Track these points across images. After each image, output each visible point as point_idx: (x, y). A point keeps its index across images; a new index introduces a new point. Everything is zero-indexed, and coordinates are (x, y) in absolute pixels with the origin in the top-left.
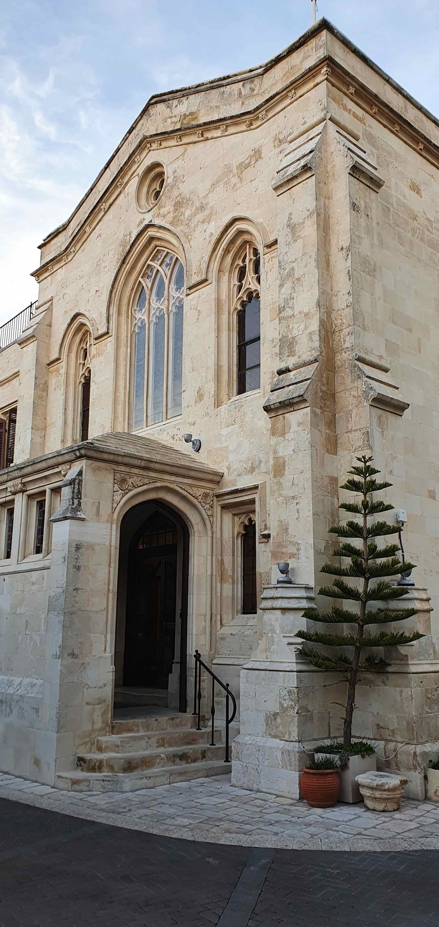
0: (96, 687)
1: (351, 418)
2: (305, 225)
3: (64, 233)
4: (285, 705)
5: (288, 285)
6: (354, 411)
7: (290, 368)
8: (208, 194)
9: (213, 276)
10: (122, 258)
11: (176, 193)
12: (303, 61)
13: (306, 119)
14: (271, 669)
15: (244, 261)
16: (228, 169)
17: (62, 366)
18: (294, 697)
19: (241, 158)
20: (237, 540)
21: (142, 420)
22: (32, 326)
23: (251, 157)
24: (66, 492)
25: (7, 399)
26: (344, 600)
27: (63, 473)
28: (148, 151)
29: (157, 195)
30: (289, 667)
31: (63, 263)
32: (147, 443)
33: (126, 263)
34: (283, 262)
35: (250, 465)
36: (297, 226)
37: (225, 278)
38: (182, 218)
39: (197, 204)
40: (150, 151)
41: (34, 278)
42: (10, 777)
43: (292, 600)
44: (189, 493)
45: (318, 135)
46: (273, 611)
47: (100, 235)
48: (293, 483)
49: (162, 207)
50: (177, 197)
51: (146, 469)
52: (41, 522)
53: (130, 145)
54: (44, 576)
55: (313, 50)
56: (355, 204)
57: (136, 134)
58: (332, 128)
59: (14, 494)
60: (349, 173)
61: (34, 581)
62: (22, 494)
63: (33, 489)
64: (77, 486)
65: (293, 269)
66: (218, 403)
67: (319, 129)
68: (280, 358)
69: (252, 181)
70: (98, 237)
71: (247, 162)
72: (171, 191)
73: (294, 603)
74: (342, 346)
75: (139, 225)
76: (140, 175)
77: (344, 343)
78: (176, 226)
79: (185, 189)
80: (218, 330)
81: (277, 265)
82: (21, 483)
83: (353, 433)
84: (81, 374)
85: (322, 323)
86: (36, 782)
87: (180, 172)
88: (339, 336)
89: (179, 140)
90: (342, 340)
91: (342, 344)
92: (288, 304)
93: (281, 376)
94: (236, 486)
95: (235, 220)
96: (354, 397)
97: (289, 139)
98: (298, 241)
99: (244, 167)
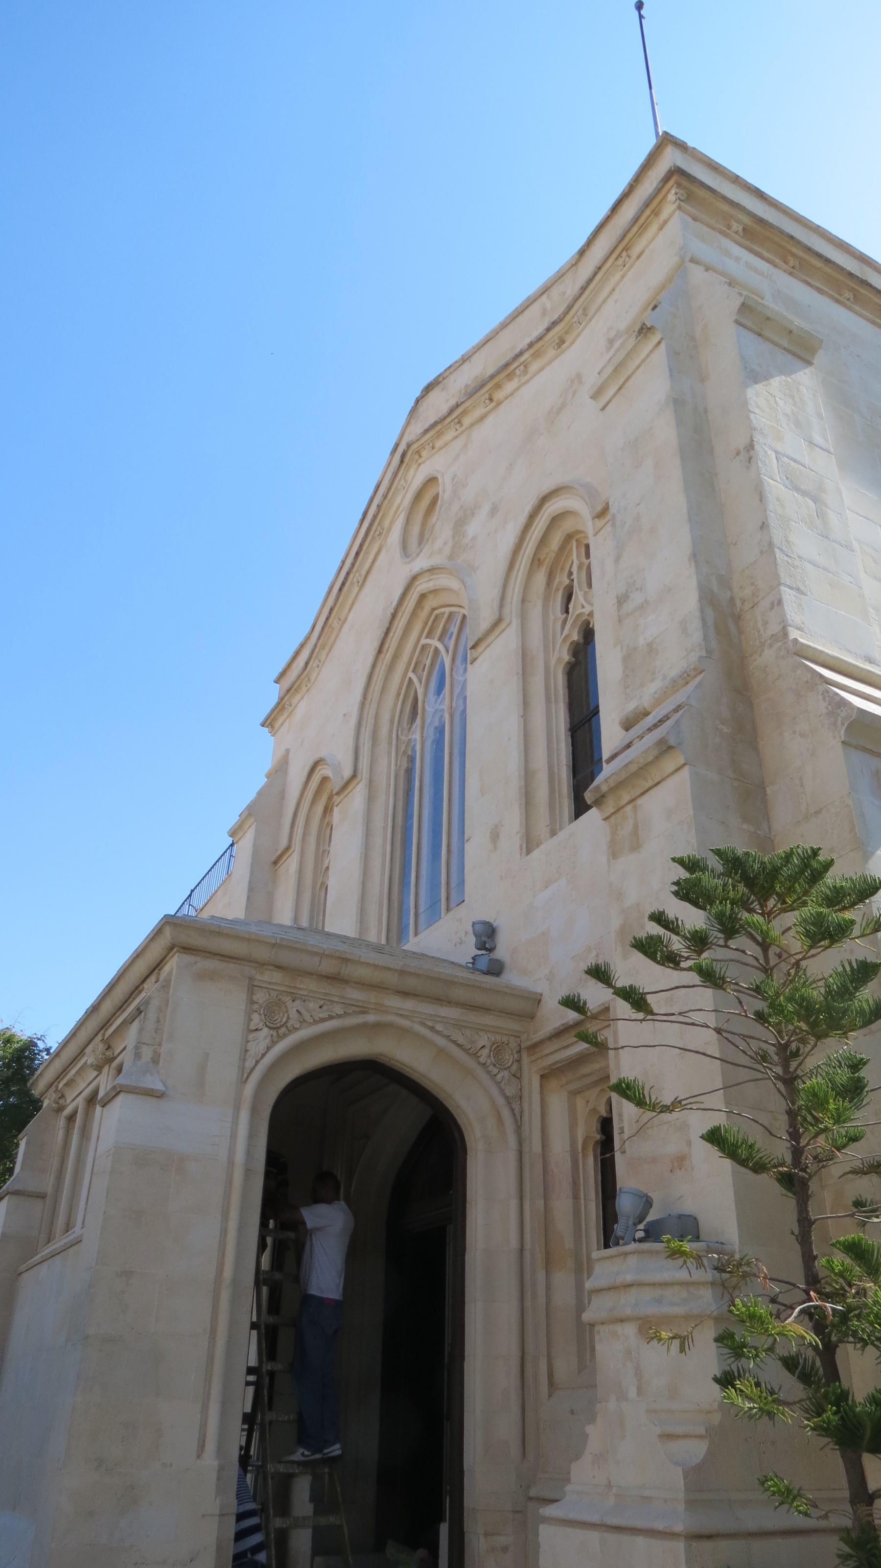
20: (585, 1156)
28: (417, 464)
40: (419, 465)
41: (267, 729)
44: (455, 1042)
51: (334, 979)
60: (737, 322)
66: (529, 844)
80: (526, 703)
85: (707, 598)
89: (458, 426)
91: (762, 632)
95: (544, 500)
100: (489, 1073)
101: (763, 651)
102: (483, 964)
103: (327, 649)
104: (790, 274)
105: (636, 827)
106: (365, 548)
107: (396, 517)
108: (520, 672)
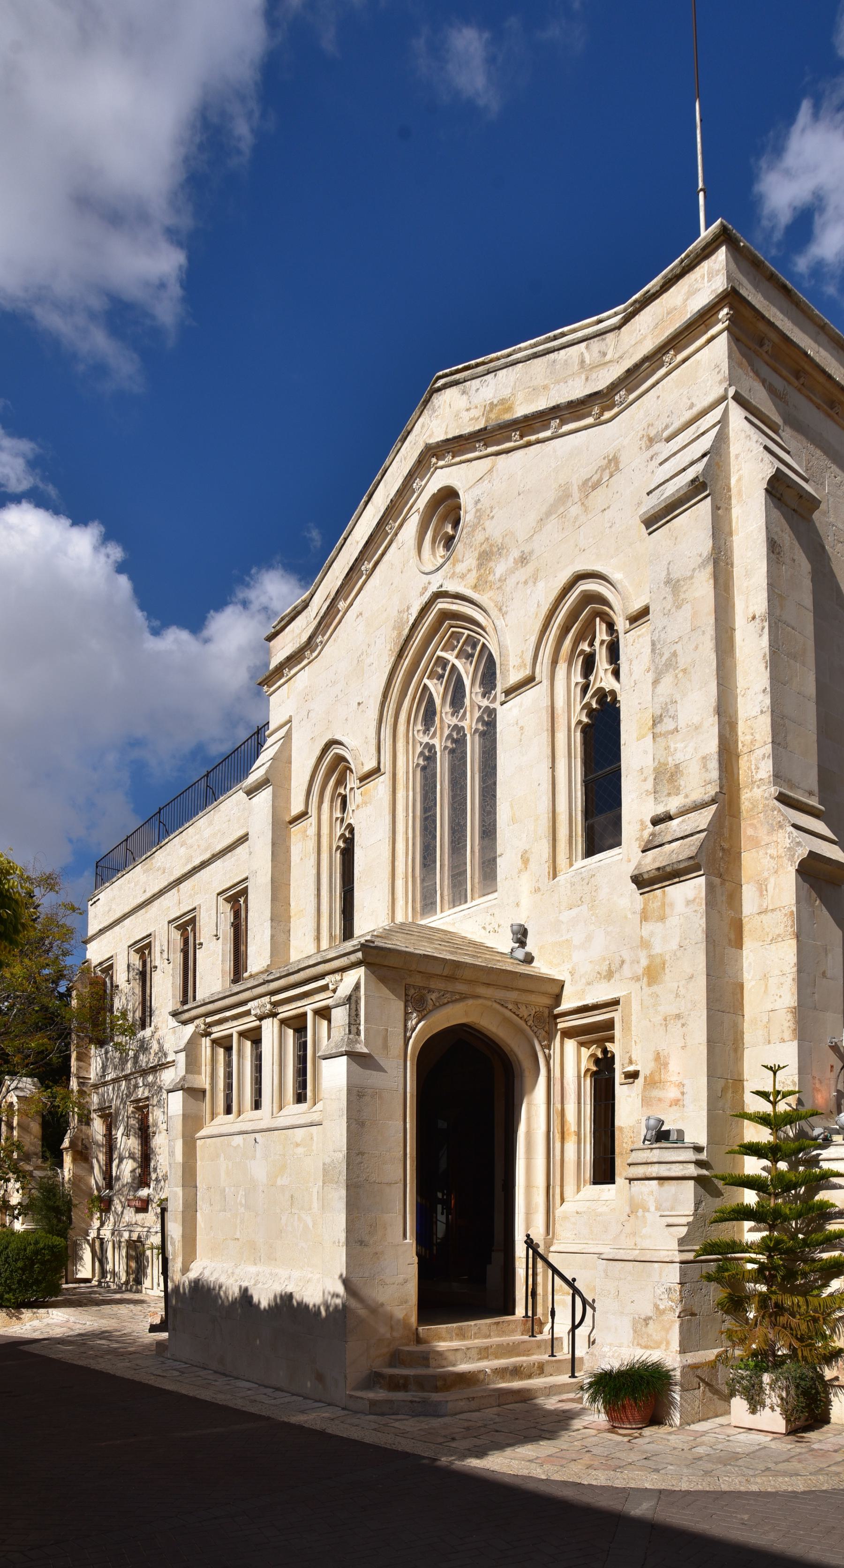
0: (394, 1284)
1: (766, 890)
2: (693, 580)
3: (304, 614)
4: (662, 1307)
5: (667, 680)
6: (772, 880)
7: (672, 813)
8: (532, 535)
9: (542, 671)
10: (397, 649)
11: (479, 537)
12: (687, 299)
13: (694, 400)
14: (642, 1259)
15: (591, 644)
16: (564, 497)
17: (311, 824)
18: (676, 1296)
19: (585, 472)
20: (585, 1081)
21: (435, 903)
22: (263, 764)
23: (602, 469)
24: (340, 1015)
25: (230, 877)
26: (746, 1157)
27: (331, 987)
29: (449, 542)
30: (668, 1256)
31: (305, 662)
32: (447, 937)
33: (404, 657)
34: (659, 642)
35: (606, 968)
36: (682, 583)
37: (562, 669)
38: (491, 578)
39: (515, 554)
42: (286, 1394)
43: (674, 1166)
45: (714, 426)
46: (647, 1182)
47: (361, 614)
48: (677, 994)
49: (458, 561)
50: (482, 544)
52: (301, 1059)
53: (403, 461)
54: (312, 1134)
55: (703, 278)
56: (775, 542)
57: (414, 442)
58: (737, 415)
59: (261, 1018)
61: (299, 1142)
63: (286, 1011)
64: (353, 1006)
65: (675, 654)
67: (715, 415)
68: (656, 798)
69: (605, 510)
70: (358, 617)
71: (595, 478)
72: (471, 534)
73: (677, 1169)
74: (752, 777)
75: (422, 594)
76: (421, 510)
77: (757, 772)
78: (481, 592)
79: (494, 529)
81: (648, 649)
82: (271, 1003)
83: (769, 914)
84: (338, 834)
86: (320, 1401)
87: (485, 503)
88: (748, 761)
90: (753, 767)
91: (754, 774)
92: (668, 711)
93: (658, 827)
94: (585, 1000)
96: (772, 857)
97: (666, 434)
98: (683, 607)
99: (591, 486)
100: (533, 1031)
101: (753, 788)
102: (520, 954)
104: (799, 390)
105: (663, 904)
108: (550, 728)
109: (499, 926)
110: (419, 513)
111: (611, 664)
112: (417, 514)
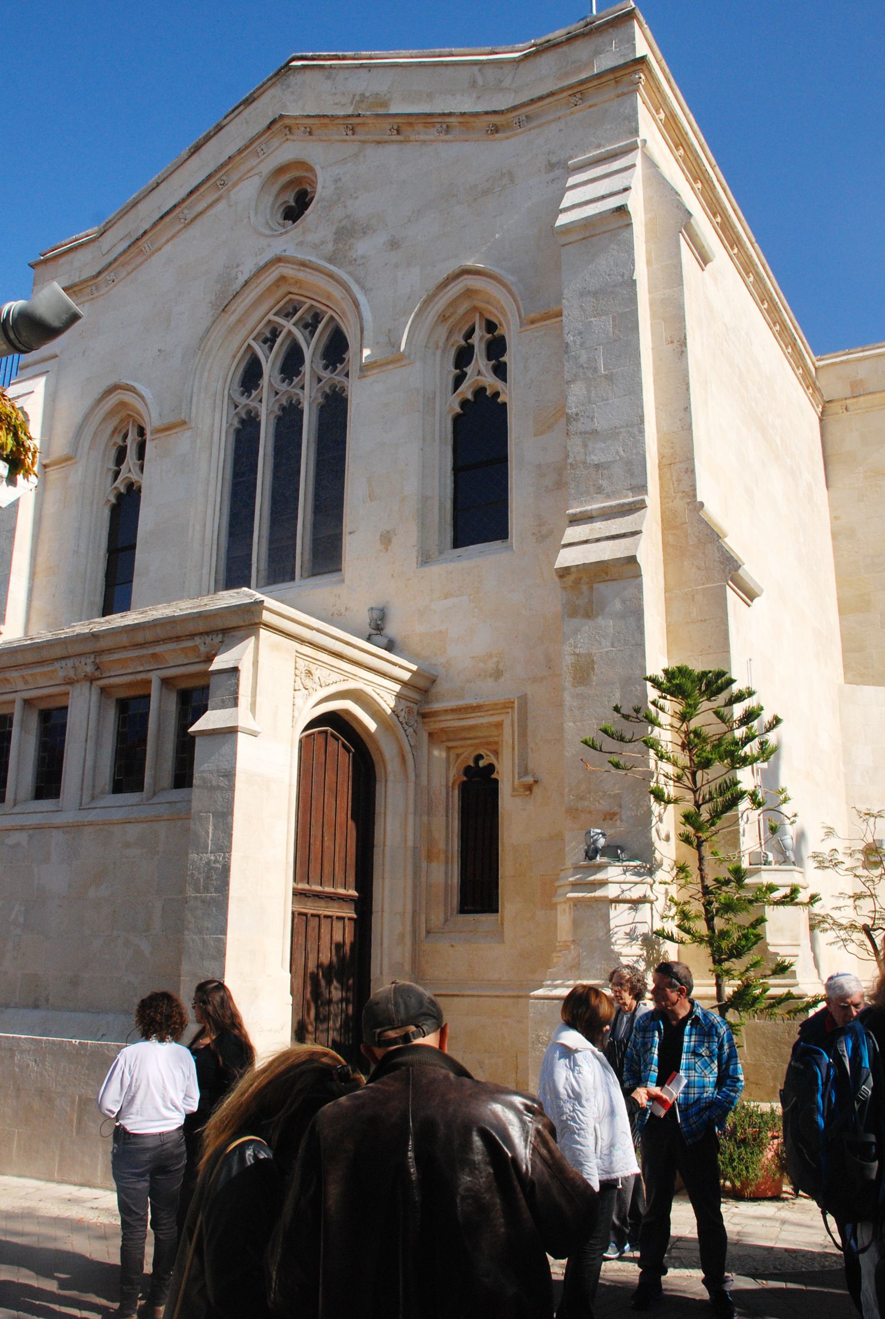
20: (453, 789)
40: (287, 140)
62: (88, 684)
76: (264, 174)
89: (350, 132)
103: (129, 268)
105: (591, 602)
106: (202, 190)
107: (246, 177)
109: (346, 609)
110: (261, 177)
111: (456, 368)
112: (257, 178)
